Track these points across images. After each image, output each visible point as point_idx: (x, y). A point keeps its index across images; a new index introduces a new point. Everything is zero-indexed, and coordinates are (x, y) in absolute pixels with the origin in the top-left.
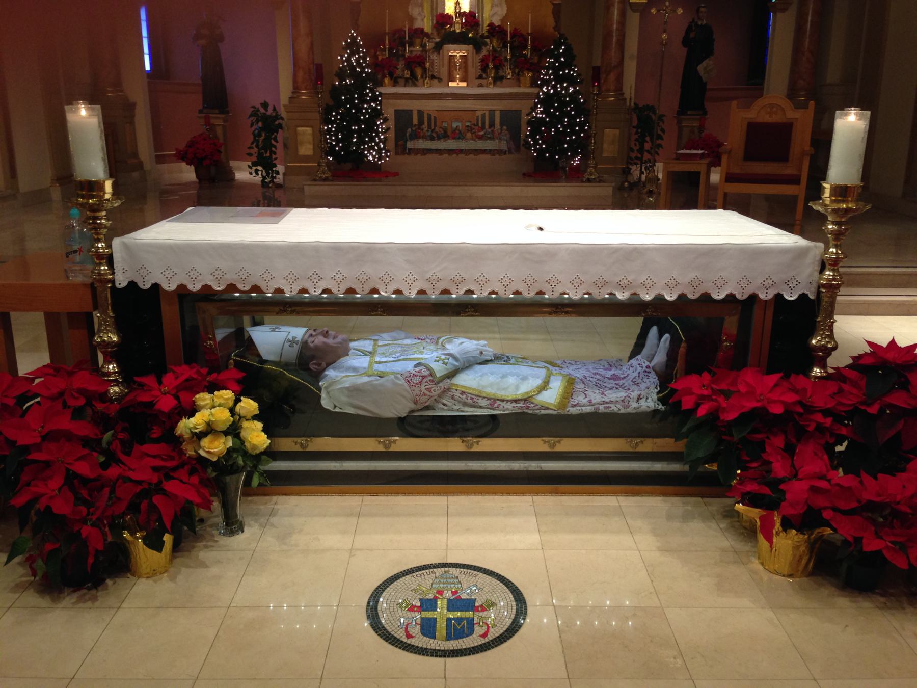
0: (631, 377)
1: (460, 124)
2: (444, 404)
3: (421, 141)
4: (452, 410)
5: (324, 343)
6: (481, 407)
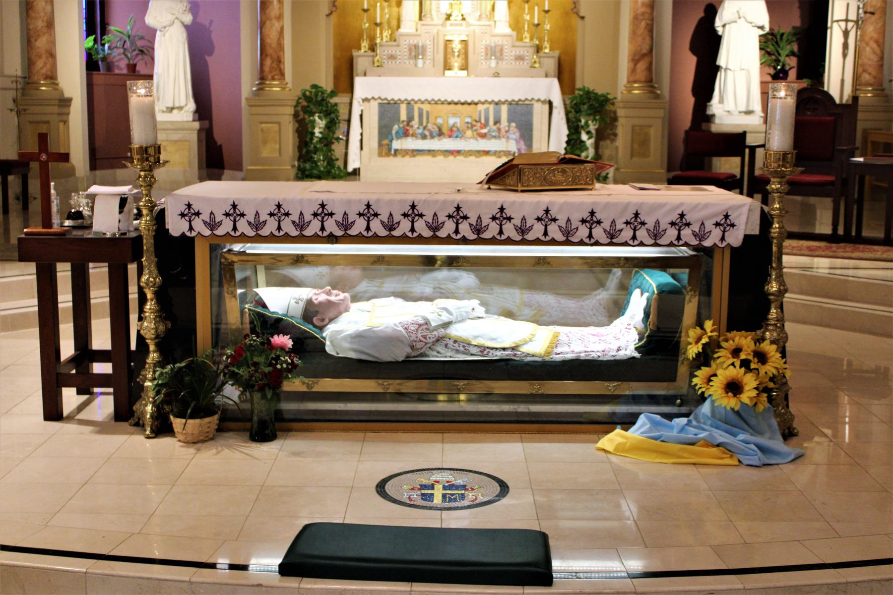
1: (457, 120)
2: (438, 352)
3: (409, 139)
4: (446, 357)
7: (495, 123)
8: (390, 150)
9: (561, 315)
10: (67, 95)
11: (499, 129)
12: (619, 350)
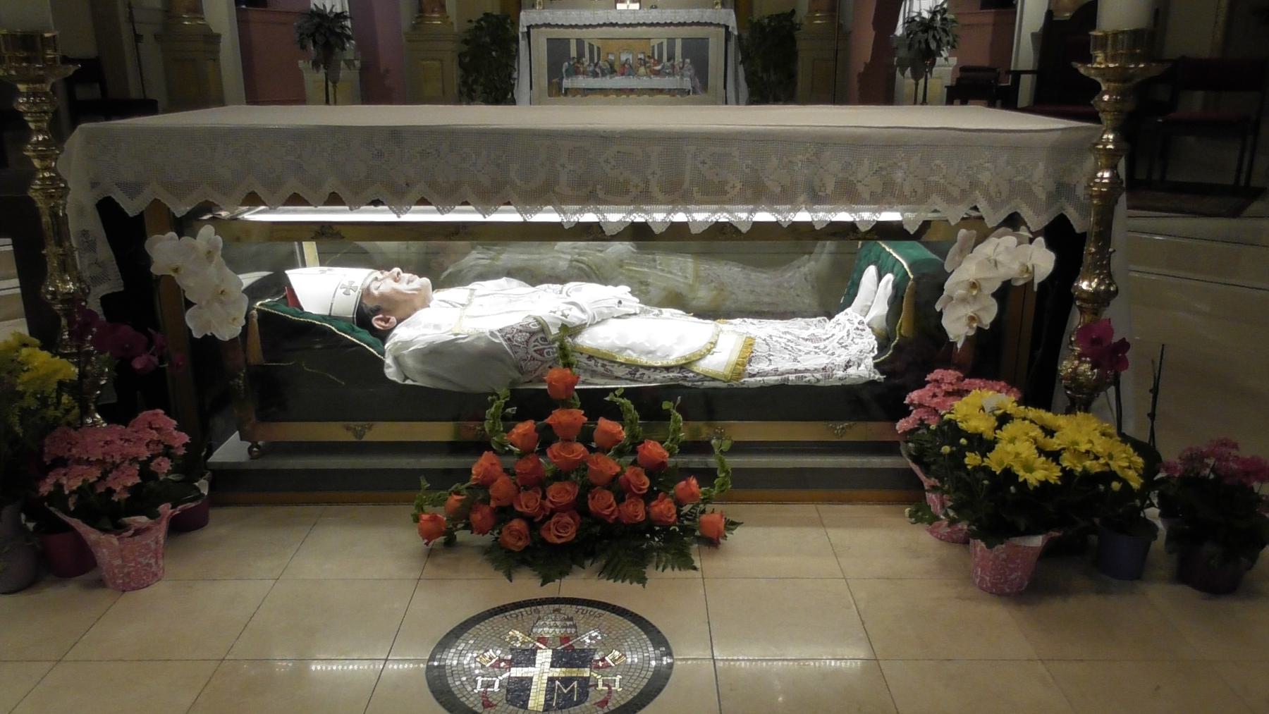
0: (836, 338)
3: (580, 78)
5: (394, 289)
6: (617, 378)
7: (669, 60)
8: (560, 89)
9: (752, 298)
10: (215, 31)
11: (673, 66)
12: (848, 366)
